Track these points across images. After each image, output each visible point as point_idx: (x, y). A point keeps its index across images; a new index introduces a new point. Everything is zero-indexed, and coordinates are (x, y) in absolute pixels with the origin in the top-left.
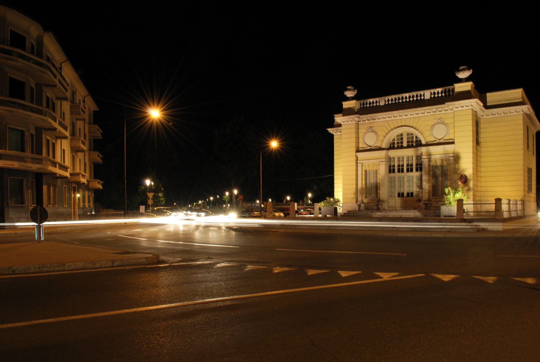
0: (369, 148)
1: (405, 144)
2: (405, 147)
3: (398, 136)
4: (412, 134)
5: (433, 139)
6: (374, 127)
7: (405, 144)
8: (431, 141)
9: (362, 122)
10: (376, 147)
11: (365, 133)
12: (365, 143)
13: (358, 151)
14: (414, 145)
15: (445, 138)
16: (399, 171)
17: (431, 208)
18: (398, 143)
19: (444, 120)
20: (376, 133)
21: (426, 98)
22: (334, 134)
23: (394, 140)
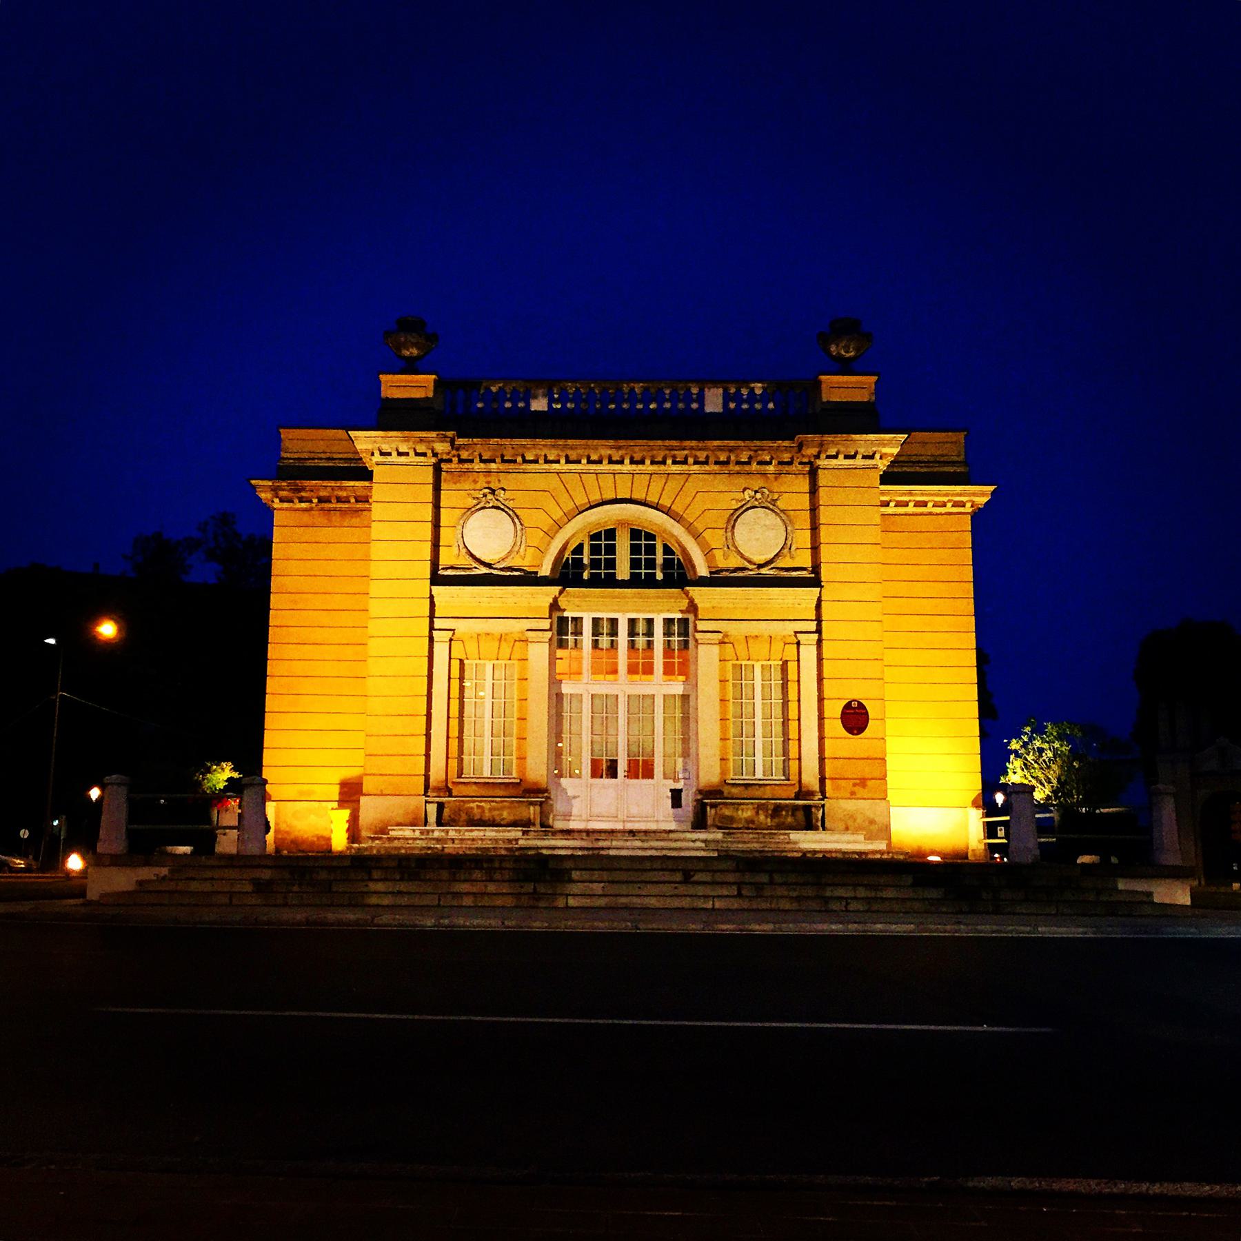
0: (484, 570)
1: (623, 571)
2: (623, 581)
3: (595, 537)
4: (650, 537)
5: (734, 562)
6: (503, 489)
7: (623, 571)
8: (727, 570)
9: (454, 466)
10: (510, 569)
11: (471, 511)
12: (465, 550)
13: (437, 579)
14: (660, 576)
15: (781, 563)
16: (632, 670)
17: (572, 818)
18: (595, 564)
19: (776, 496)
20: (514, 516)
21: (709, 409)
22: (277, 504)
23: (579, 549)
